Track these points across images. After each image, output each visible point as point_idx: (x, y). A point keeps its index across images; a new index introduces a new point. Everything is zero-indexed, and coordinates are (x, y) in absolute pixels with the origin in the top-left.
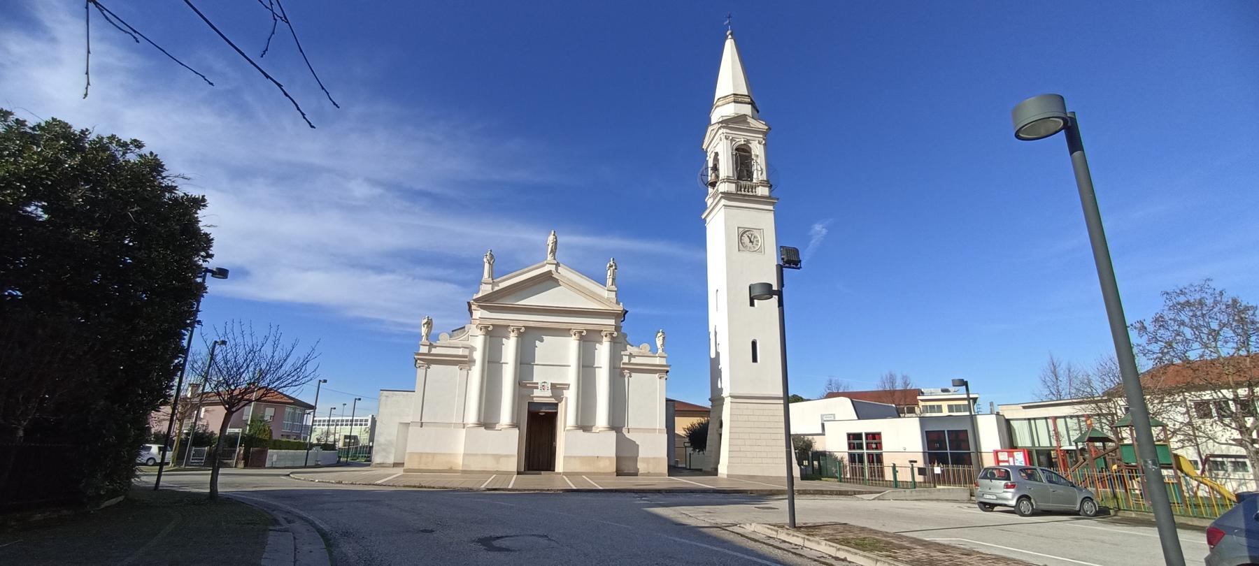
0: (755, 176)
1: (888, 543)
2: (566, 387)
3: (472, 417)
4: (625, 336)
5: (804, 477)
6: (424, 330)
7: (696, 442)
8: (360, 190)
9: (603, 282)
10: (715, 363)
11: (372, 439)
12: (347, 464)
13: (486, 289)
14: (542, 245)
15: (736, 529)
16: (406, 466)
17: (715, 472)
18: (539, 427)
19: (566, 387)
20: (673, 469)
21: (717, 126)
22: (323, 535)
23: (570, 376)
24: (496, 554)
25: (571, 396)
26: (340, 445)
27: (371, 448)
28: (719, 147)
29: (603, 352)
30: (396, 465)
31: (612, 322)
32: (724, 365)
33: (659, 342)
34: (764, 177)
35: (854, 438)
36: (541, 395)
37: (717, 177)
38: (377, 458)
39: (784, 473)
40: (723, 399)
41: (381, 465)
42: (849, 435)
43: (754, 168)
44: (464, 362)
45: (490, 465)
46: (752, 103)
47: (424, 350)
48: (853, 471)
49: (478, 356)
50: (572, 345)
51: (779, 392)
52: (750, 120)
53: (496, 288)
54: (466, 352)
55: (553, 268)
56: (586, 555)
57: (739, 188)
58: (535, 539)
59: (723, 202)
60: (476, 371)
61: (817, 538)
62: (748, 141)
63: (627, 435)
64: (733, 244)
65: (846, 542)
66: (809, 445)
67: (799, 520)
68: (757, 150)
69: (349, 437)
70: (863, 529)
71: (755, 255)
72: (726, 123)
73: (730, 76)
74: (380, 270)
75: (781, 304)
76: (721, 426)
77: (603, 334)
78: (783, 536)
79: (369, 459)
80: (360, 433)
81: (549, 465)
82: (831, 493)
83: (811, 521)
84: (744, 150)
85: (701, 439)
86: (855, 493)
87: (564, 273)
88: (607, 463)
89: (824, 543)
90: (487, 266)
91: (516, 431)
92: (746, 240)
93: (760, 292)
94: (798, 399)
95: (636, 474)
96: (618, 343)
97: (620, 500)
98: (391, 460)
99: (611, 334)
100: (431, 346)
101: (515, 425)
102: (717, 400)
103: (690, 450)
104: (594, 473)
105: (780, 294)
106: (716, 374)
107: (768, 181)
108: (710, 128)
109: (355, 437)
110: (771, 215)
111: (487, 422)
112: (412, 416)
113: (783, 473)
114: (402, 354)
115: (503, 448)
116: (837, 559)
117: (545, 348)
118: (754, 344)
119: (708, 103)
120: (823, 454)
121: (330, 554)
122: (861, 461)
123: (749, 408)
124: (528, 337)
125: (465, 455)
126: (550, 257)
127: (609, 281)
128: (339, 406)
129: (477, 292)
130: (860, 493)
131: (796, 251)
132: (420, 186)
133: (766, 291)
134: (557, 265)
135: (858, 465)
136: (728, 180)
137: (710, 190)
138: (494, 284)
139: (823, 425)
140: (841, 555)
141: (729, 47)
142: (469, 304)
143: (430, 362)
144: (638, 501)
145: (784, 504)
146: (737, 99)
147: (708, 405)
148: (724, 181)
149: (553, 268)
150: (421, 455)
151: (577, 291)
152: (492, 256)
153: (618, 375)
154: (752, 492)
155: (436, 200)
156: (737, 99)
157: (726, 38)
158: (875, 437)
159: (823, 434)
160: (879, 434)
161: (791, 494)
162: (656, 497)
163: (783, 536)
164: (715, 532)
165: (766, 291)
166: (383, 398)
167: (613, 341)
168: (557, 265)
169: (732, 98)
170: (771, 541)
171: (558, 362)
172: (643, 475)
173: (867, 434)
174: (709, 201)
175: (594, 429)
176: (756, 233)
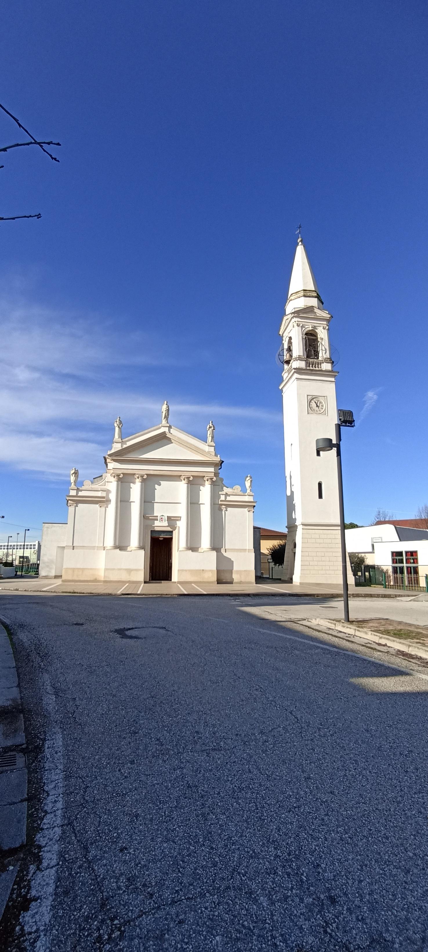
0: (320, 355)
1: (419, 633)
2: (179, 518)
3: (110, 542)
4: (222, 480)
5: (358, 584)
6: (72, 479)
7: (277, 559)
8: (23, 375)
9: (205, 440)
10: (290, 499)
11: (38, 559)
12: (22, 577)
13: (117, 447)
14: (159, 412)
15: (305, 623)
16: (64, 578)
17: (290, 581)
18: (160, 550)
19: (179, 518)
20: (259, 579)
21: (290, 316)
22: (6, 626)
23: (181, 511)
24: (128, 640)
25: (182, 527)
26: (16, 563)
27: (38, 565)
28: (292, 333)
29: (205, 493)
30: (56, 577)
31: (212, 469)
32: (297, 501)
33: (248, 484)
34: (328, 355)
35: (397, 556)
36: (160, 525)
37: (291, 356)
38: (43, 572)
39: (341, 581)
40: (296, 526)
41: (46, 577)
42: (393, 553)
43: (320, 349)
44: (103, 501)
45: (124, 577)
46: (318, 297)
47: (73, 493)
48: (396, 579)
49: (113, 497)
50: (182, 487)
51: (338, 521)
52: (316, 310)
53: (125, 446)
54: (104, 494)
55: (166, 429)
56: (193, 642)
57: (308, 364)
58: (155, 629)
59: (296, 376)
60: (112, 508)
61: (365, 630)
62: (315, 327)
63: (225, 554)
64: (305, 407)
65: (387, 632)
66: (362, 560)
67: (352, 617)
68: (322, 334)
69: (23, 557)
70: (400, 623)
71: (320, 416)
72: (298, 313)
73: (301, 275)
74: (40, 434)
75: (339, 454)
76: (295, 547)
77: (205, 479)
78: (339, 627)
79: (37, 573)
80: (30, 554)
81: (167, 577)
82: (378, 596)
83: (361, 616)
84: (312, 335)
85: (278, 556)
86: (396, 596)
87: (175, 433)
88: (210, 574)
89: (370, 633)
90: (117, 429)
91: (142, 552)
92: (313, 405)
93: (325, 445)
94: (353, 526)
95: (231, 583)
96: (217, 485)
97: (219, 603)
98: (53, 574)
99: (212, 479)
100: (78, 490)
101: (141, 547)
102: (292, 527)
103: (272, 565)
104: (200, 582)
105: (338, 446)
106: (291, 508)
107: (330, 359)
108: (285, 318)
109: (27, 558)
110: (333, 385)
111: (121, 545)
112: (66, 542)
113: (340, 581)
114: (55, 496)
115: (133, 564)
116: (379, 644)
117: (163, 490)
118: (320, 485)
119: (283, 297)
120: (373, 567)
121: (11, 640)
122: (402, 572)
123: (316, 533)
124: (150, 482)
125: (106, 570)
126: (164, 422)
127: (209, 439)
128: (14, 535)
129: (111, 449)
130: (400, 596)
131: (351, 413)
132: (66, 370)
133: (327, 444)
134: (170, 427)
135: (399, 575)
136: (299, 358)
137: (286, 366)
138: (122, 443)
139: (373, 546)
140: (383, 642)
141: (300, 252)
142: (105, 459)
143: (77, 502)
144: (234, 602)
145: (340, 604)
146: (306, 294)
147: (285, 531)
148: (296, 359)
149: (166, 429)
150: (73, 570)
151: (184, 446)
152: (121, 422)
153: (217, 509)
154: (318, 595)
155: (79, 380)
156: (306, 294)
157: (297, 244)
158: (412, 555)
159: (373, 552)
160: (416, 552)
161: (346, 596)
162: (247, 599)
163: (339, 627)
164: (289, 625)
165: (327, 444)
166: (45, 529)
167: (213, 484)
168: (170, 427)
169: (302, 293)
170: (330, 632)
171: (172, 501)
172: (237, 583)
173: (407, 553)
174: (285, 375)
175: (200, 550)
176: (322, 400)
